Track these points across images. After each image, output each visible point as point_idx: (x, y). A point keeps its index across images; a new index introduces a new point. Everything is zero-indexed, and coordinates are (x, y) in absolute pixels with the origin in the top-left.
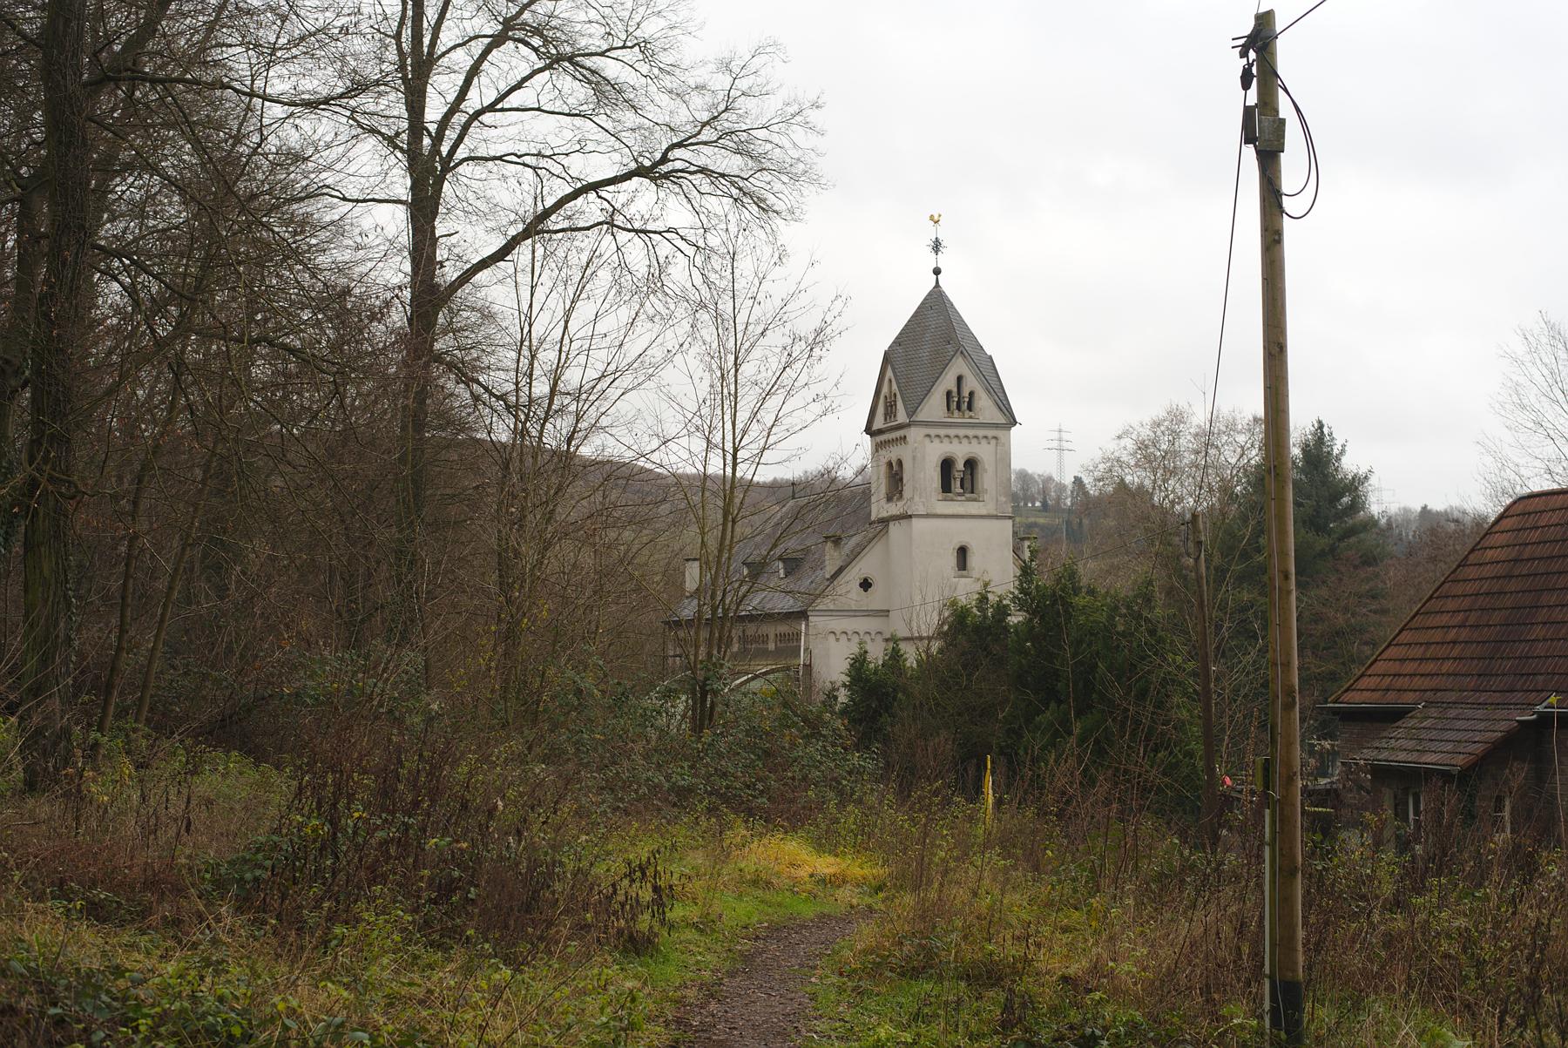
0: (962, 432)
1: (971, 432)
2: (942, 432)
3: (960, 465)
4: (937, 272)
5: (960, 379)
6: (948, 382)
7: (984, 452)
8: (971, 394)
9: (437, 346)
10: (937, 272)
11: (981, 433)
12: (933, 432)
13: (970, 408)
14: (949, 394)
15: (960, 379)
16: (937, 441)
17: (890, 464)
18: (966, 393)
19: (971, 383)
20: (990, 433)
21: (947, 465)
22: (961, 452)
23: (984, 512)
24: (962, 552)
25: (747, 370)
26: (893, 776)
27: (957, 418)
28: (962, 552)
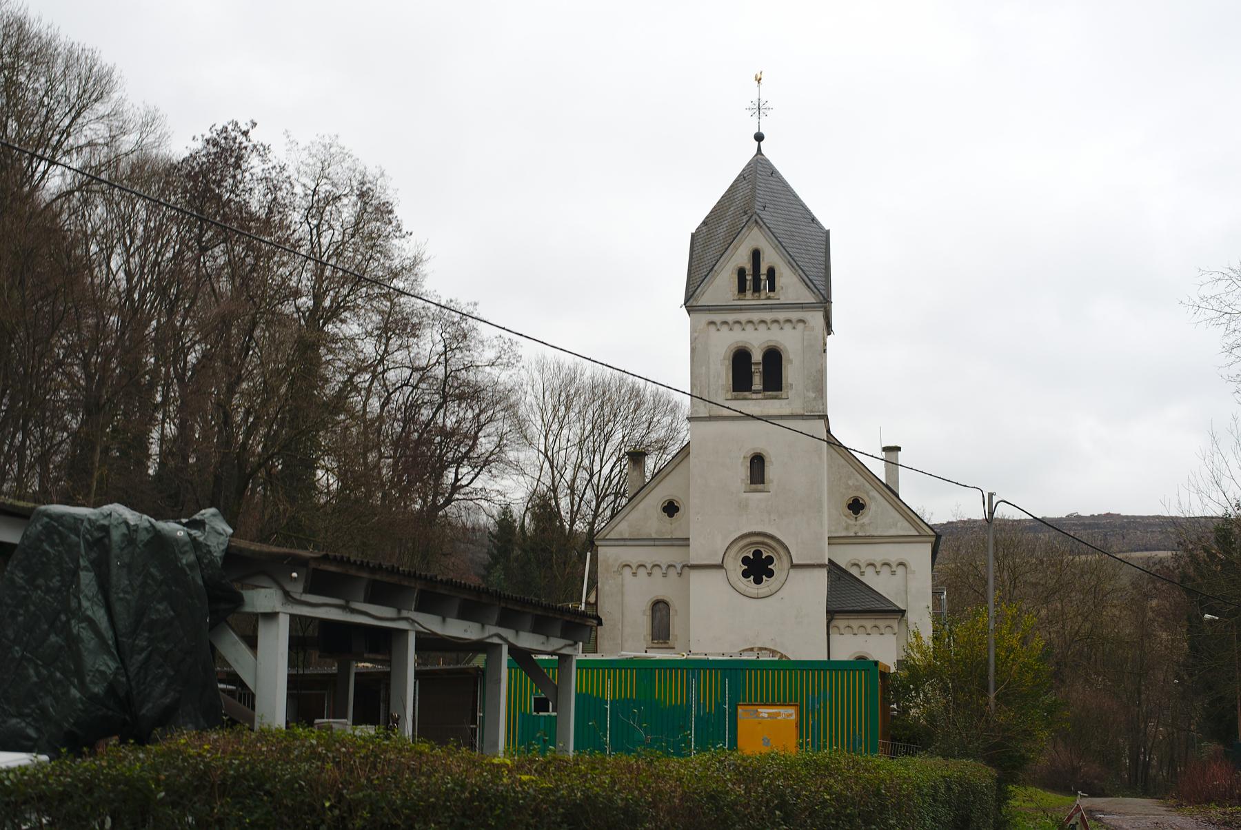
0: (756, 316)
1: (768, 316)
2: (730, 317)
3: (757, 356)
4: (759, 137)
5: (756, 255)
6: (740, 257)
7: (789, 340)
8: (771, 273)
9: (254, 206)
10: (759, 137)
11: (781, 316)
12: (718, 318)
13: (772, 289)
14: (741, 273)
15: (756, 255)
16: (725, 328)
18: (763, 270)
19: (770, 258)
20: (795, 315)
21: (741, 359)
22: (757, 341)
23: (787, 411)
24: (757, 464)
25: (97, 105)
26: (517, 552)
27: (750, 299)
28: (757, 464)
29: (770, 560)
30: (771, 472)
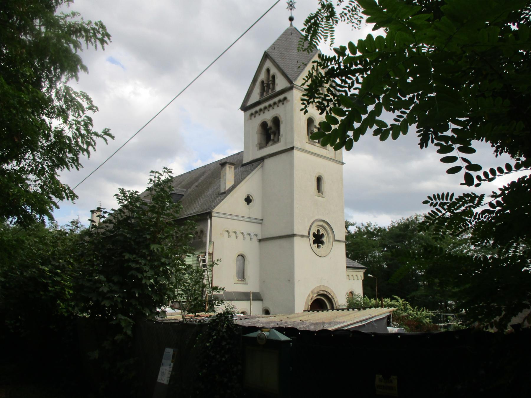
17: (264, 125)
29: (322, 243)
30: (325, 186)
